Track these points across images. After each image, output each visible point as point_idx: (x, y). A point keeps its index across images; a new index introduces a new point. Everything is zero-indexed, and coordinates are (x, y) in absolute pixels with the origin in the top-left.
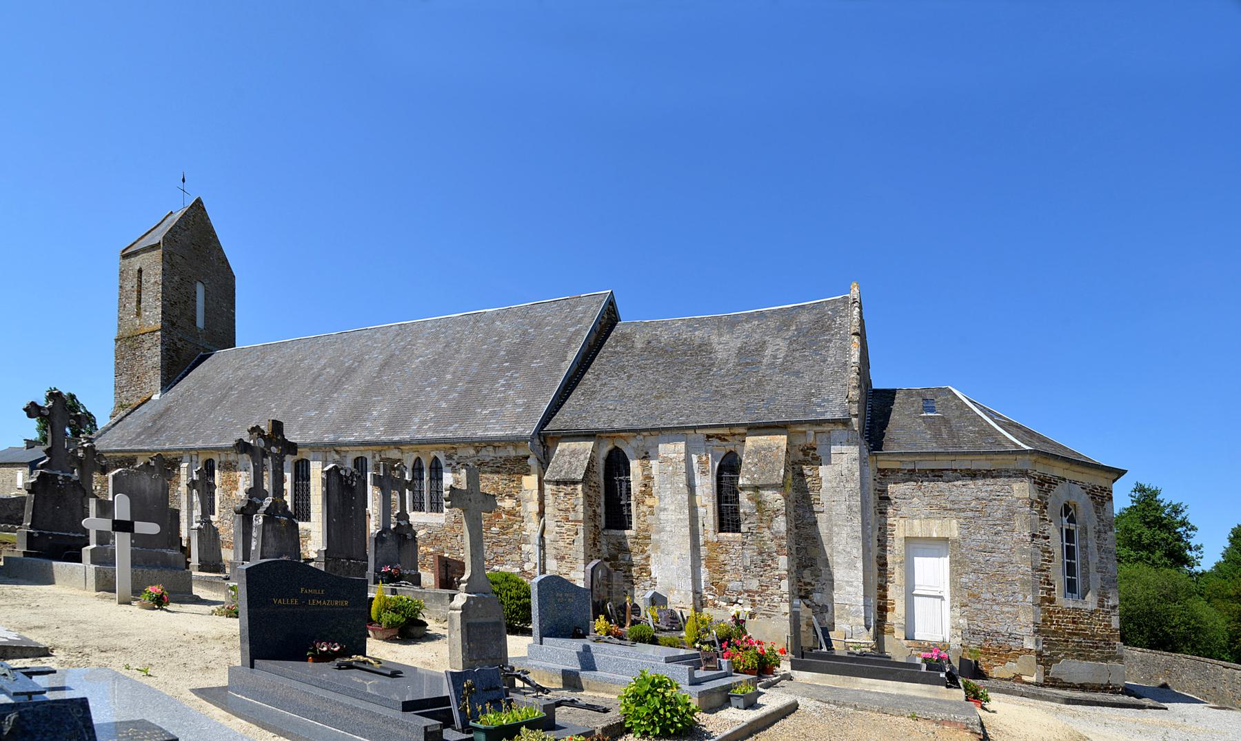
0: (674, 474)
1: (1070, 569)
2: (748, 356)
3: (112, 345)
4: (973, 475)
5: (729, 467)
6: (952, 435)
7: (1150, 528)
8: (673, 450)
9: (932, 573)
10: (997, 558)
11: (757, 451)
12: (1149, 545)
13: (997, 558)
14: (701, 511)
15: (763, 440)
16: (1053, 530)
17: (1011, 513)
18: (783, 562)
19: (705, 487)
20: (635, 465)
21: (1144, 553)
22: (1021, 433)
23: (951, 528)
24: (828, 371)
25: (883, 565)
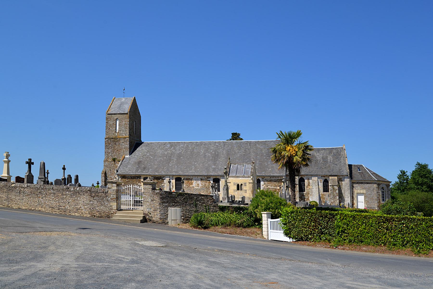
0: (315, 182)
1: (383, 197)
2: (325, 159)
3: (104, 140)
4: (368, 183)
5: (326, 182)
6: (364, 176)
7: (422, 178)
8: (315, 179)
9: (361, 198)
10: (371, 196)
11: (332, 179)
12: (421, 183)
13: (371, 196)
14: (320, 189)
15: (333, 177)
16: (380, 191)
17: (374, 189)
18: (338, 197)
19: (321, 185)
20: (306, 181)
21: (419, 187)
22: (375, 175)
23: (364, 191)
24: (342, 165)
25: (353, 197)
